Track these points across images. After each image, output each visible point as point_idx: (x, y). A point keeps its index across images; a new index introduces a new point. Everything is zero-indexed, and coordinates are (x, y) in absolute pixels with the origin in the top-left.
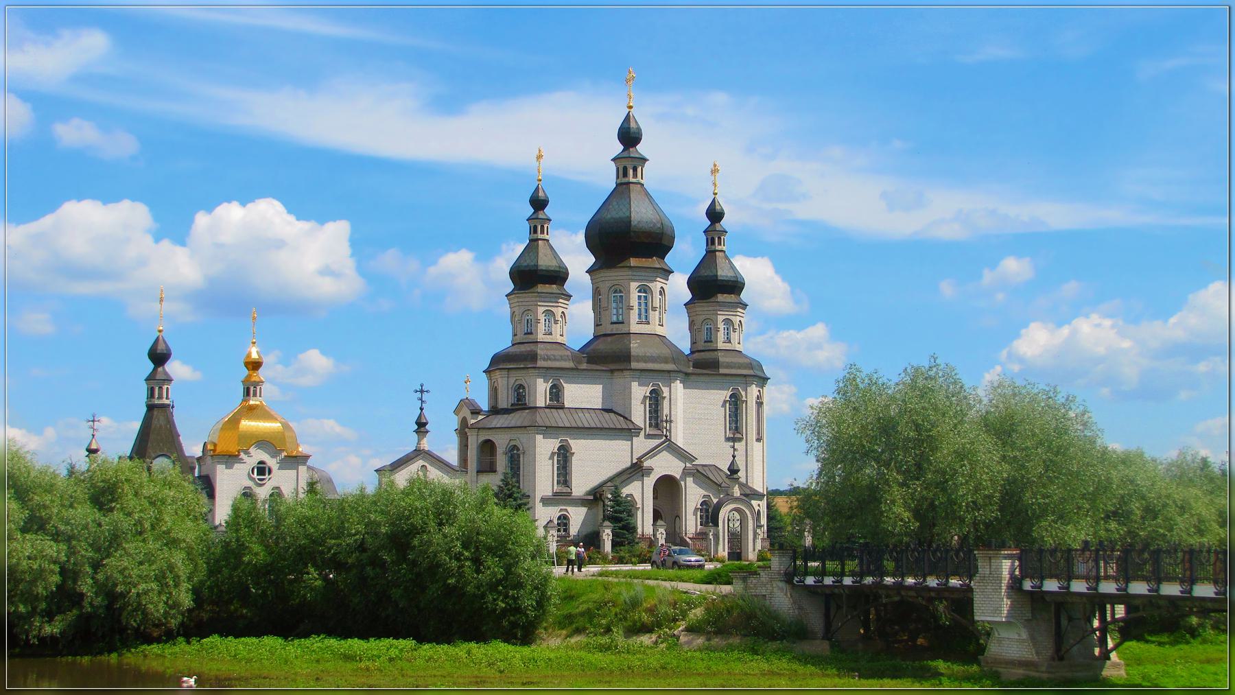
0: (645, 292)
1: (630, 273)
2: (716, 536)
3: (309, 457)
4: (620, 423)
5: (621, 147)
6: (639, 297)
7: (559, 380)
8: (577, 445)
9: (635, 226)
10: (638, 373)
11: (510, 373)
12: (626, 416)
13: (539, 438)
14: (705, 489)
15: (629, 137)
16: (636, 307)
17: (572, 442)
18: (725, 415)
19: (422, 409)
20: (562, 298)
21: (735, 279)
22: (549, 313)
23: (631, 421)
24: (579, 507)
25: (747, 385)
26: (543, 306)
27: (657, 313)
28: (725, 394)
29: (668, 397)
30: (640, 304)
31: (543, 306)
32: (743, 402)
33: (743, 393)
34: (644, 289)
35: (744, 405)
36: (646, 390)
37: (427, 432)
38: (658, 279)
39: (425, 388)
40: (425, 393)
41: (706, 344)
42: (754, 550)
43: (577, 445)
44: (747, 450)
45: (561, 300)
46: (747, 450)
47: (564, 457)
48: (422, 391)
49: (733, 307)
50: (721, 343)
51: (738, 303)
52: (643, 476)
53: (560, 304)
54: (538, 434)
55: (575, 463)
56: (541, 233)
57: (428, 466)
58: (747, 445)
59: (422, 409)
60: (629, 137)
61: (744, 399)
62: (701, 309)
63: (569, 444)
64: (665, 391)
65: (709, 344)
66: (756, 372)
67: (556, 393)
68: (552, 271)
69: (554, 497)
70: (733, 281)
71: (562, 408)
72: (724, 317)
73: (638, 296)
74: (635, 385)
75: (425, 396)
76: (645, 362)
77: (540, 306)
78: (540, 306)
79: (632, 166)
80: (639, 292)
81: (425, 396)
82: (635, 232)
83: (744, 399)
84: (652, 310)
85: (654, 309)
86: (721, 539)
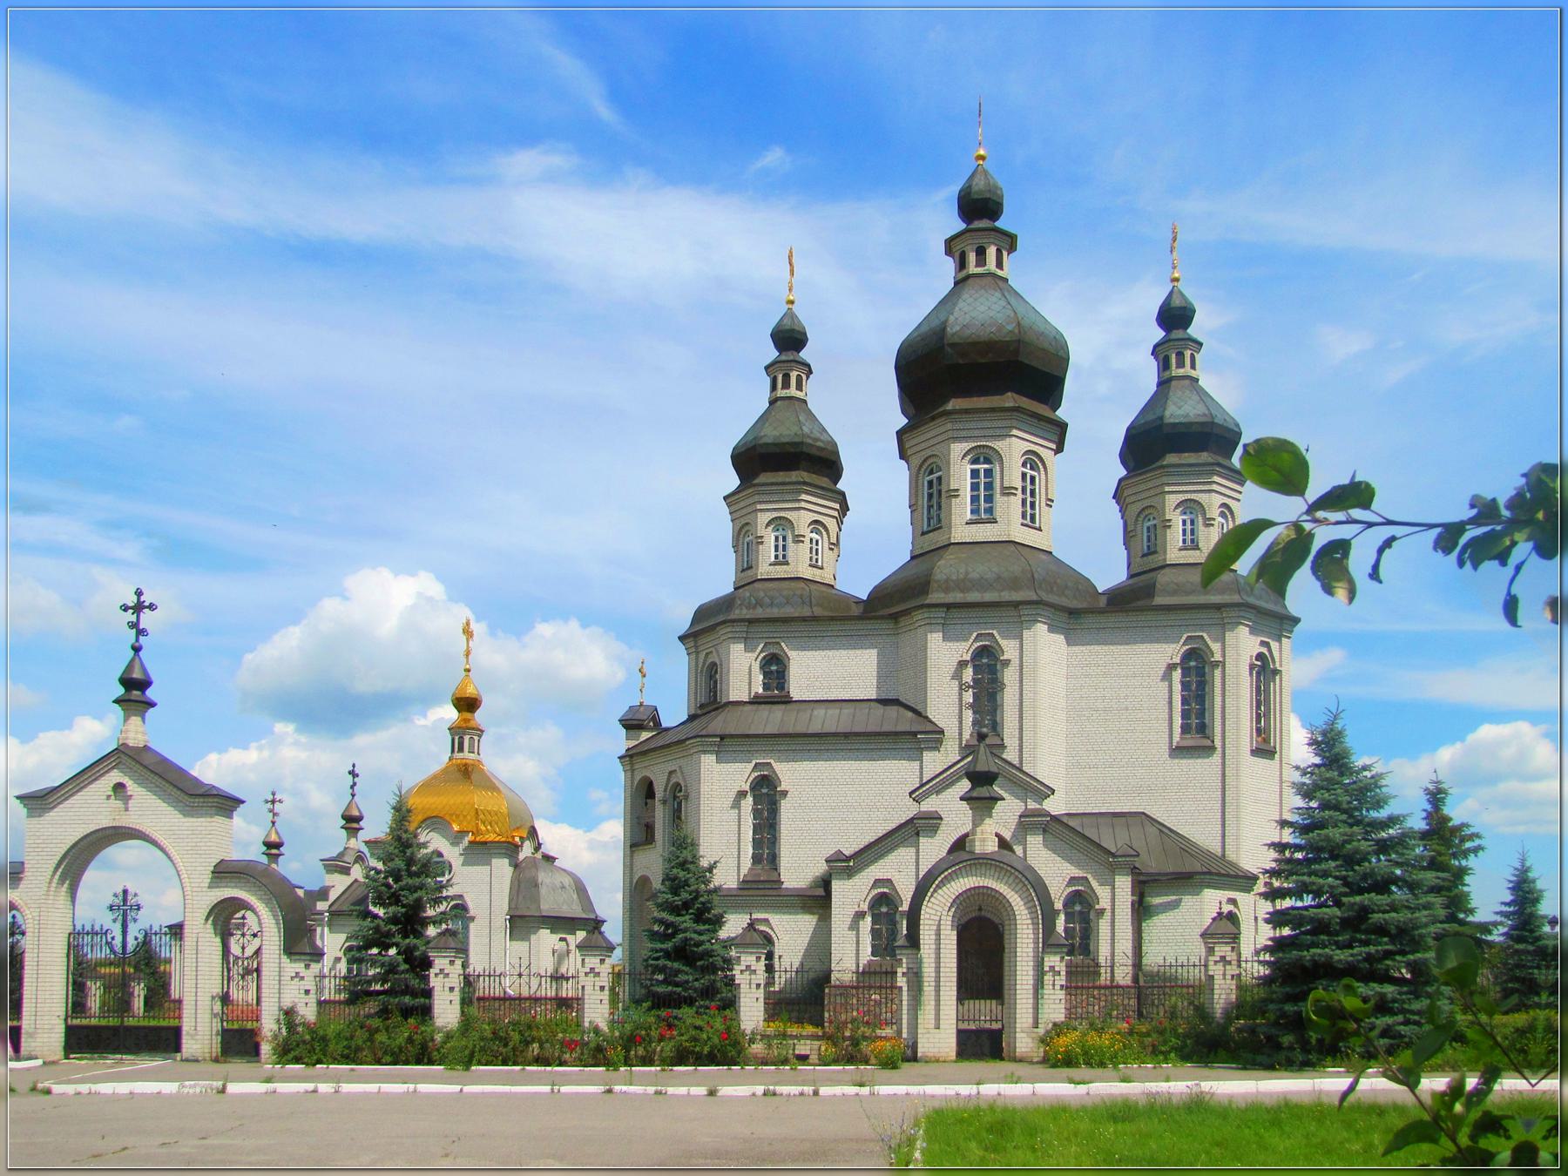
0: (987, 461)
1: (949, 426)
2: (915, 977)
3: (243, 802)
4: (905, 721)
5: (1164, 334)
6: (975, 474)
7: (778, 643)
8: (791, 773)
9: (953, 335)
10: (941, 613)
11: (700, 643)
12: (918, 708)
13: (708, 761)
14: (1077, 864)
15: (1174, 317)
16: (967, 493)
17: (778, 767)
18: (1170, 698)
19: (137, 649)
20: (807, 493)
21: (1209, 420)
22: (780, 523)
23: (927, 717)
24: (798, 914)
25: (1222, 628)
26: (768, 510)
27: (1016, 501)
28: (1172, 651)
29: (1015, 662)
30: (975, 487)
31: (768, 510)
32: (1216, 664)
33: (1215, 647)
34: (983, 456)
35: (1218, 672)
36: (963, 649)
37: (152, 704)
38: (1015, 432)
39: (147, 598)
40: (146, 610)
41: (1145, 558)
42: (1036, 1024)
43: (791, 773)
44: (1224, 775)
45: (804, 497)
46: (1224, 775)
47: (766, 793)
48: (139, 608)
49: (1200, 474)
50: (1176, 551)
51: (1213, 464)
52: (918, 834)
53: (803, 505)
54: (705, 752)
55: (788, 812)
56: (782, 388)
57: (132, 787)
58: (1224, 764)
59: (137, 649)
60: (1174, 317)
61: (1217, 657)
62: (1134, 490)
63: (774, 772)
64: (1009, 648)
65: (1150, 557)
66: (1245, 597)
67: (775, 669)
68: (787, 443)
69: (741, 893)
70: (1202, 424)
71: (786, 700)
72: (1182, 497)
73: (972, 471)
74: (935, 640)
75: (147, 619)
76: (962, 591)
77: (761, 510)
78: (761, 510)
79: (975, 247)
80: (975, 461)
81: (147, 619)
82: (953, 345)
83: (1217, 657)
84: (1003, 494)
85: (1008, 491)
86: (928, 988)
